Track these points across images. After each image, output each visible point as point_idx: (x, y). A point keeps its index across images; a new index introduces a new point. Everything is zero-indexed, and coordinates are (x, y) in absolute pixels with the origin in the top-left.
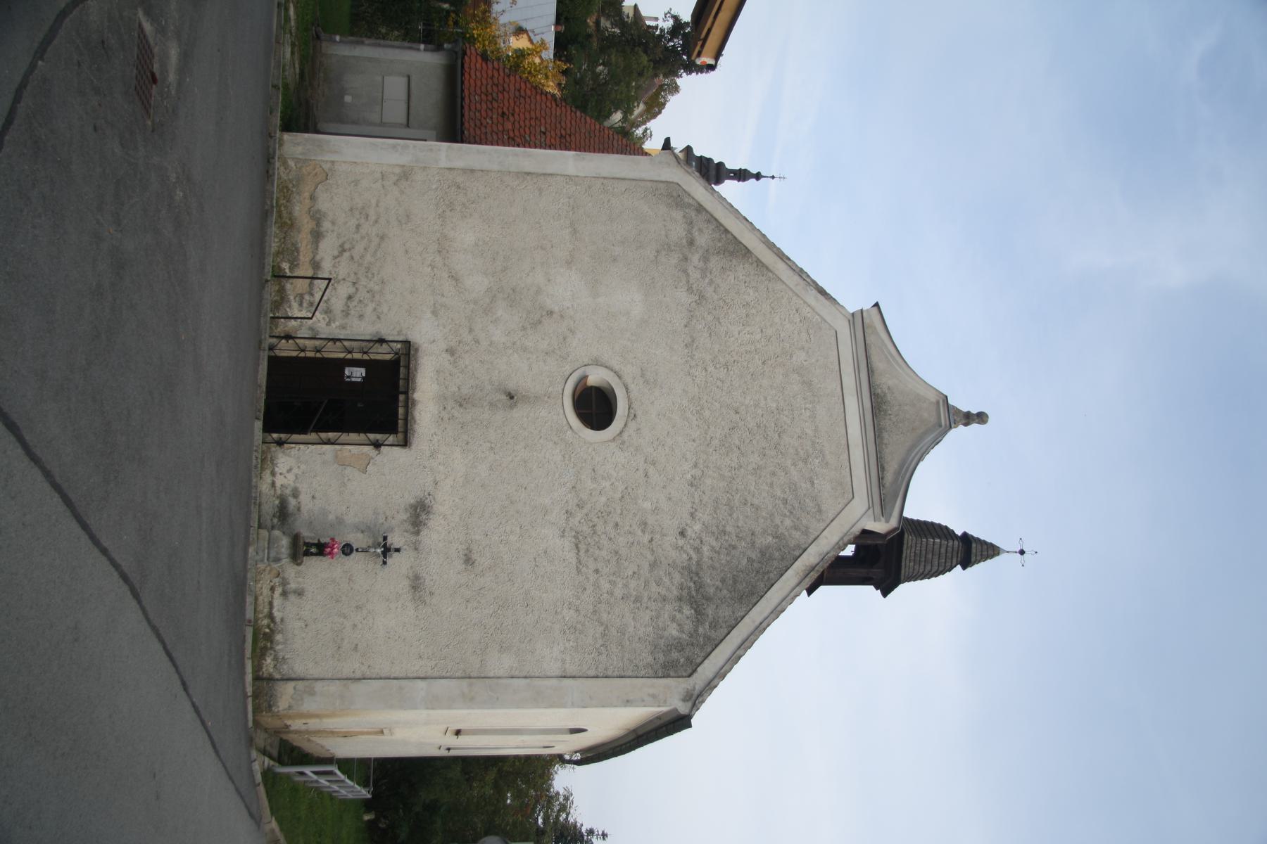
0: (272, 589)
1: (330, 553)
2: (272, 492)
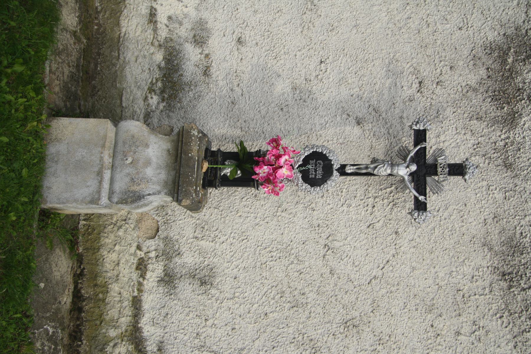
0: (142, 266)
1: (269, 180)
2: (149, 34)
